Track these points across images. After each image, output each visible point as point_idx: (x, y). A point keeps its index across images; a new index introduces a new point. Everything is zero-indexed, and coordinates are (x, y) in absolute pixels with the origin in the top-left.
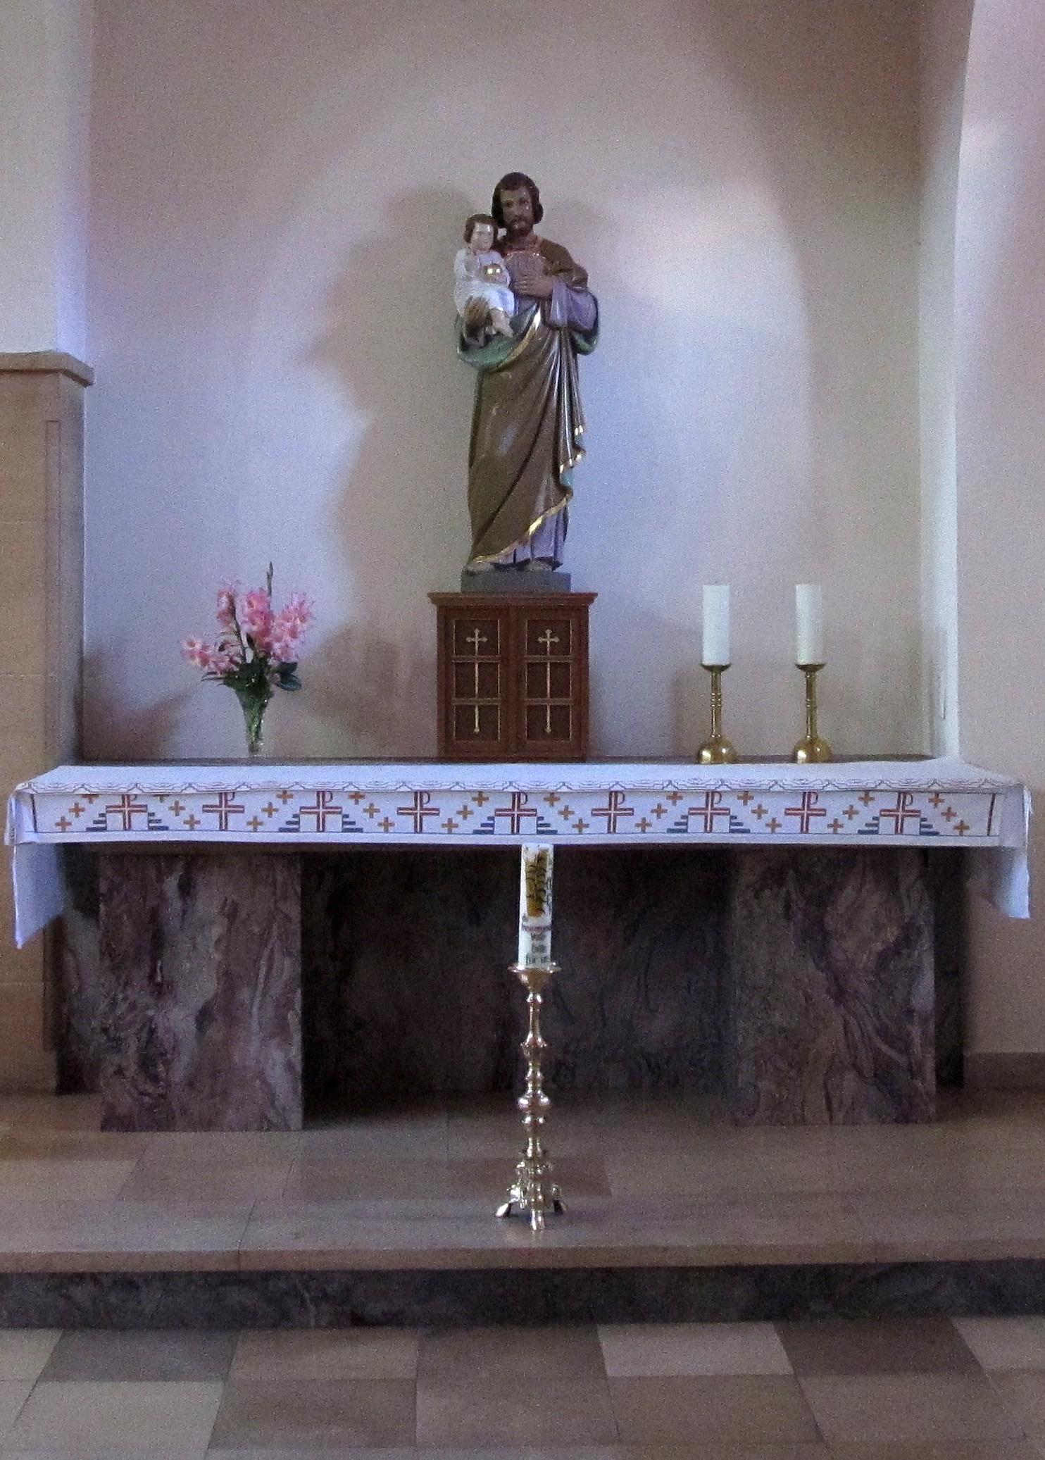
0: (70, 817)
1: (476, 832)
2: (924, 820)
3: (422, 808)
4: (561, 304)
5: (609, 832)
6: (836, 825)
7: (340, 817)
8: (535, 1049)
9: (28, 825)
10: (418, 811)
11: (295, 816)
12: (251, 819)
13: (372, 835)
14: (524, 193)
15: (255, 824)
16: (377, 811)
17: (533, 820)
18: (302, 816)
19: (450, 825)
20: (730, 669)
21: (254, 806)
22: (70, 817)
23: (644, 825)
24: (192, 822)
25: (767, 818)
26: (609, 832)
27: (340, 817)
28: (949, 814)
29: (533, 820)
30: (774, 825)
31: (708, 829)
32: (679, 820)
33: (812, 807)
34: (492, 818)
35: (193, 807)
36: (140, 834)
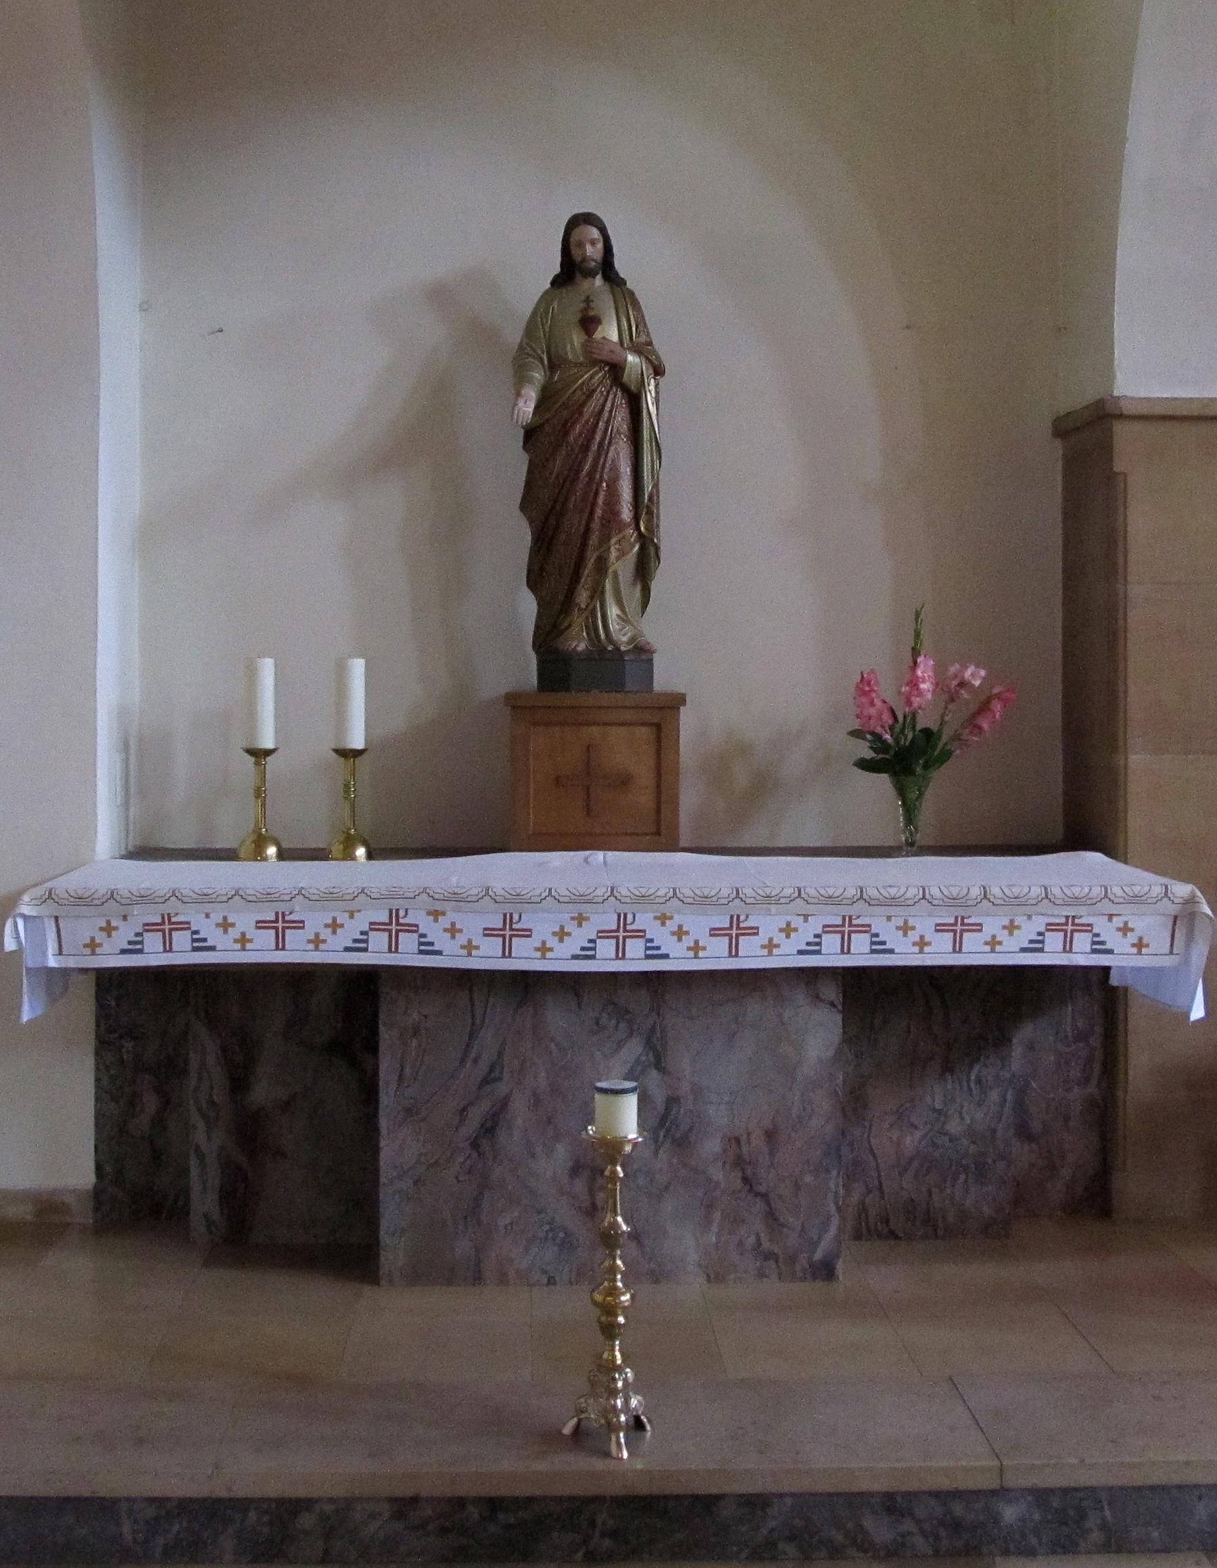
0: (100, 937)
1: (347, 949)
2: (196, 932)
3: (398, 924)
4: (572, 344)
5: (390, 951)
6: (770, 946)
7: (188, 933)
8: (623, 1294)
9: (52, 947)
10: (394, 927)
11: (816, 936)
12: (312, 937)
13: (226, 953)
14: (595, 233)
15: (993, 943)
16: (233, 925)
17: (641, 943)
18: (824, 937)
19: (544, 949)
20: (365, 756)
21: (316, 922)
22: (100, 937)
23: (770, 946)
24: (922, 943)
25: (462, 939)
26: (390, 951)
27: (867, 936)
28: (1125, 930)
29: (641, 943)
30: (922, 943)
31: (845, 950)
32: (812, 939)
33: (401, 921)
34: (365, 933)
35: (924, 925)
36: (183, 955)
